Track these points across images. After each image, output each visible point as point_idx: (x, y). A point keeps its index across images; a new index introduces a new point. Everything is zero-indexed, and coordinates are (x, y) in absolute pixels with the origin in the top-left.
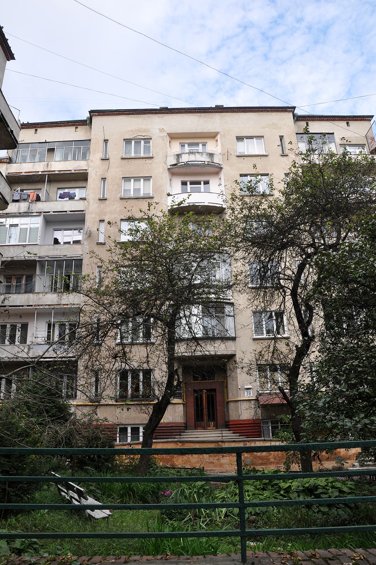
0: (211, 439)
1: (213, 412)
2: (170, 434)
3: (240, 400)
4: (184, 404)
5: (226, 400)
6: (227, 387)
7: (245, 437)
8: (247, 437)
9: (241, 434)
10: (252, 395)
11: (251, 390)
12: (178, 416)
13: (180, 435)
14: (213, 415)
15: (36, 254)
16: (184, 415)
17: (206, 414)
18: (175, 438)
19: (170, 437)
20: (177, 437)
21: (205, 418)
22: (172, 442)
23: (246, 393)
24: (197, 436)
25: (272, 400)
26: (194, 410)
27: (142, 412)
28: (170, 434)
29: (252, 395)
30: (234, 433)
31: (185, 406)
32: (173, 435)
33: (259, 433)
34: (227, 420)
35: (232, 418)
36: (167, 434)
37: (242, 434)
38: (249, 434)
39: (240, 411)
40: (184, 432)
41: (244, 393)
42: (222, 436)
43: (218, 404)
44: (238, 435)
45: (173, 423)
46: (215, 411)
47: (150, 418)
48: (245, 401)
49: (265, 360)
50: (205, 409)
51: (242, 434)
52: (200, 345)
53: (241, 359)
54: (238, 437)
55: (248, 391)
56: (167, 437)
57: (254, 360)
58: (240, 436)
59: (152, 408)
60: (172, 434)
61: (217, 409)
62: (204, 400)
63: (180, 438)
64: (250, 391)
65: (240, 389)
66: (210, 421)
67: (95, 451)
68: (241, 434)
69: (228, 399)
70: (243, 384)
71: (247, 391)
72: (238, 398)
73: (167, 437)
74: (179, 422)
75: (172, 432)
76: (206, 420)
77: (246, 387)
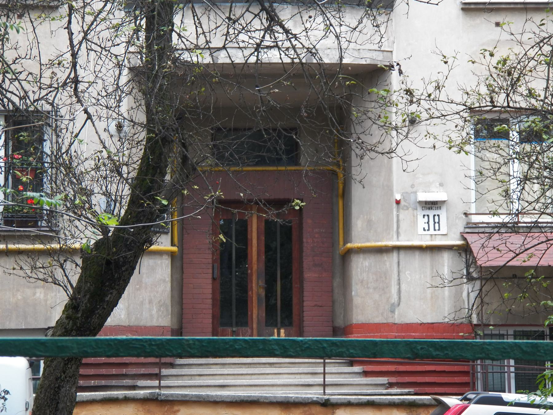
0: (280, 394)
1: (287, 291)
2: (114, 371)
3: (398, 248)
4: (172, 255)
5: (342, 248)
6: (346, 194)
7: (412, 390)
8: (417, 389)
9: (393, 380)
10: (443, 230)
11: (444, 209)
12: (150, 302)
13: (158, 377)
14: (287, 305)
15: (445, 57)
16: (172, 297)
17: (259, 295)
18: (134, 387)
19: (114, 382)
20: (141, 383)
21: (255, 312)
22: (127, 400)
23: (422, 222)
24: (221, 382)
25: (544, 246)
26: (214, 279)
27: (41, 276)
28: (114, 371)
29: (443, 230)
30: (366, 374)
31: (178, 264)
32: (125, 376)
33: (465, 379)
34: (340, 322)
35: (354, 322)
36: (103, 371)
37: (407, 379)
38: (427, 379)
39: (394, 290)
40: (172, 365)
41: (414, 223)
42: (324, 385)
43: (307, 262)
44: (384, 380)
45: (129, 327)
46: (295, 286)
47: (72, 298)
48: (417, 254)
49: (525, 93)
50: (254, 278)
51: (407, 379)
52: (283, 27)
53: (434, 84)
54: (385, 391)
55: (431, 213)
56: (103, 382)
57: (484, 90)
58: (391, 385)
59: (80, 262)
60: (124, 371)
61: (301, 280)
62: (255, 242)
63: (160, 387)
64: (436, 212)
65: (398, 202)
66: (276, 326)
67: (151, 345)
68: (393, 380)
69: (347, 239)
70: (412, 186)
71: (427, 212)
72: (391, 239)
73: (103, 382)
74: (155, 323)
75: (125, 365)
76: (259, 322)
77: (423, 197)
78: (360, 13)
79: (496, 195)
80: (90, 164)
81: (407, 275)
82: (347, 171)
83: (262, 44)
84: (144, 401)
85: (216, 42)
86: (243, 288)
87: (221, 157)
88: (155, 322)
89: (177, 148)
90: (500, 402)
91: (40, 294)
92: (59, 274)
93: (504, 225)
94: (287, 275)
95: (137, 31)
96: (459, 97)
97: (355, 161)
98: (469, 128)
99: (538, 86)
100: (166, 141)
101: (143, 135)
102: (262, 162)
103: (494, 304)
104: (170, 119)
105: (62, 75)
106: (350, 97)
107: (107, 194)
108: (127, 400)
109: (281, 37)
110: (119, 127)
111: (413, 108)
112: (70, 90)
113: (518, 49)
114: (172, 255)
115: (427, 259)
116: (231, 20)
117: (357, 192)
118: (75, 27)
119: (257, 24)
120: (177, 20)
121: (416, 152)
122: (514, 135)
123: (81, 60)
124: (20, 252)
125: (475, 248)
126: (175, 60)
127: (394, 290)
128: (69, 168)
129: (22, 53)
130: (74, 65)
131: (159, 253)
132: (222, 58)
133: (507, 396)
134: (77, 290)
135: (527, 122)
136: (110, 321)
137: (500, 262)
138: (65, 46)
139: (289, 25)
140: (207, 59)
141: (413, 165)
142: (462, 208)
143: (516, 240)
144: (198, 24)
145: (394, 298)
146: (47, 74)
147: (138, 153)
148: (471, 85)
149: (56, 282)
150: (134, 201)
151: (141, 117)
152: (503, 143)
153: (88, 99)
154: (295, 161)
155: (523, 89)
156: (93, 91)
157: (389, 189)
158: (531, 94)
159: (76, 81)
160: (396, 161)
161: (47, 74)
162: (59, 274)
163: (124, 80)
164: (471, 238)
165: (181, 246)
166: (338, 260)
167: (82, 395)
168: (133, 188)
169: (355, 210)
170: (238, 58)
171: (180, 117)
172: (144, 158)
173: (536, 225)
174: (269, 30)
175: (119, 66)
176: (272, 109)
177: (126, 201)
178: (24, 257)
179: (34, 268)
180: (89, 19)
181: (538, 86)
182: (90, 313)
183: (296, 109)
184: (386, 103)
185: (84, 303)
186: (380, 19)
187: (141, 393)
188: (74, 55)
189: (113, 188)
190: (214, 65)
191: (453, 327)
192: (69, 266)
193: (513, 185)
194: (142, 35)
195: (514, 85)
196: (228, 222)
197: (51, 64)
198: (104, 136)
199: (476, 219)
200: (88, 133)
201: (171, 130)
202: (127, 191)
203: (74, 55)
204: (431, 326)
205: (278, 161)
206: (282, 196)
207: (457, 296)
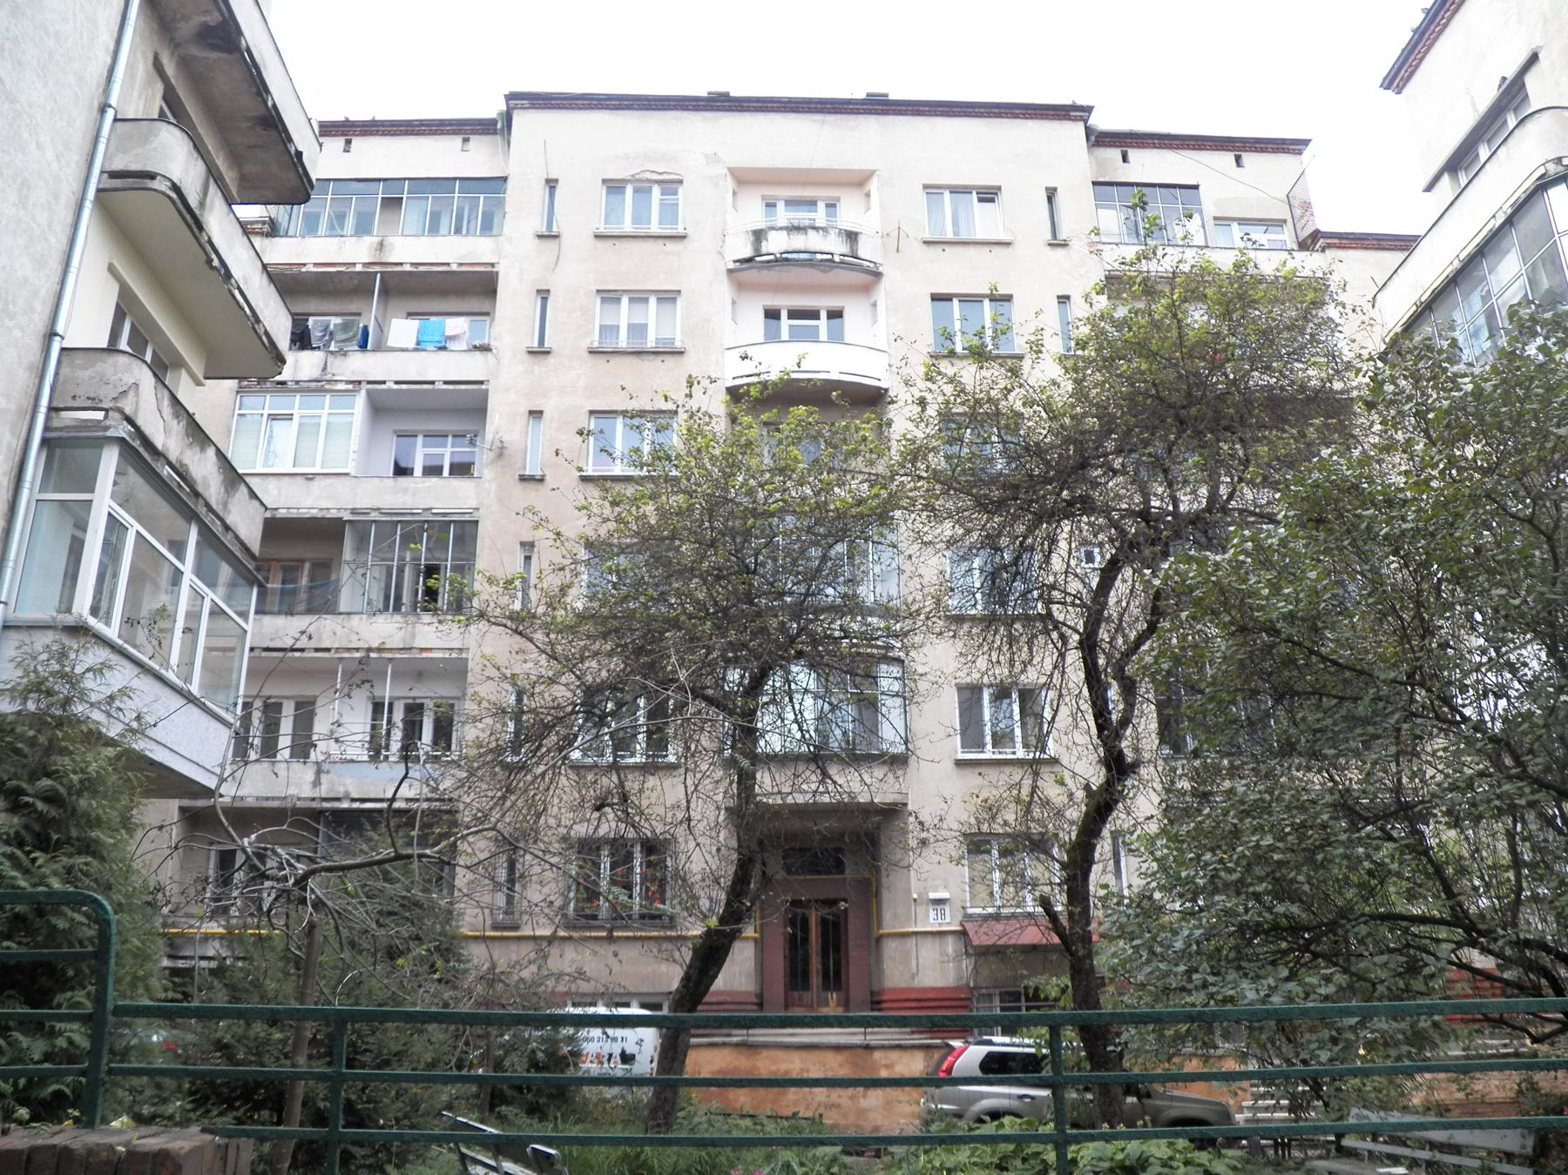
4: (755, 940)
5: (876, 933)
6: (878, 894)
14: (838, 974)
22: (724, 1044)
23: (932, 914)
29: (948, 919)
34: (876, 988)
39: (914, 963)
41: (927, 915)
43: (851, 943)
57: (973, 821)
69: (880, 926)
77: (932, 895)
78: (886, 768)
79: (984, 895)
80: (699, 877)
81: (923, 953)
82: (878, 881)
83: (765, 248)
84: (737, 1045)
85: (786, 789)
86: (806, 961)
87: (789, 871)
88: (744, 989)
89: (758, 866)
90: (990, 1043)
91: (663, 967)
92: (677, 954)
93: (990, 915)
94: (837, 949)
95: (731, 783)
96: (955, 826)
97: (884, 873)
98: (964, 848)
99: (1011, 817)
100: (751, 860)
101: (735, 856)
102: (819, 873)
103: (985, 972)
104: (754, 846)
105: (680, 816)
106: (878, 828)
107: (711, 899)
108: (724, 1044)
109: (831, 788)
110: (718, 850)
111: (924, 835)
112: (685, 826)
113: (995, 792)
114: (755, 940)
115: (937, 940)
116: (796, 776)
117: (885, 894)
118: (689, 782)
119: (813, 778)
120: (758, 776)
121: (926, 867)
122: (995, 853)
123: (692, 805)
124: (641, 938)
125: (971, 934)
126: (757, 804)
127: (914, 963)
128: (684, 880)
129: (653, 800)
130: (688, 808)
131: (747, 939)
132: (790, 800)
133: (995, 1039)
134: (690, 967)
135: (1007, 842)
136: (714, 988)
137: (990, 943)
138: (682, 795)
139: (836, 778)
140: (780, 801)
141: (924, 876)
142: (960, 904)
143: (999, 927)
144: (774, 779)
145: (914, 969)
146: (670, 814)
147: (732, 870)
148: (964, 818)
149: (674, 961)
150: (728, 904)
151: (734, 844)
152: (986, 857)
153: (696, 832)
154: (842, 872)
155: (1000, 820)
156: (701, 826)
157: (909, 892)
158: (1006, 823)
159: (689, 819)
160: (912, 873)
161: (670, 814)
162: (677, 954)
163: (721, 818)
164: (968, 926)
165: (762, 933)
166: (873, 942)
167: (694, 1041)
168: (728, 894)
169: (885, 906)
170: (800, 799)
171: (761, 843)
172: (736, 873)
173: (1014, 916)
174: (822, 782)
175: (718, 808)
176: (824, 837)
177: (723, 904)
178: (652, 943)
179: (660, 951)
180: (699, 776)
181: (1011, 817)
182: (699, 983)
183: (842, 835)
184: (905, 832)
185: (694, 977)
186: (900, 773)
187: (735, 1039)
188: (688, 802)
189: (714, 895)
190: (785, 805)
191: (956, 989)
192: (683, 949)
193: (996, 888)
194: (735, 786)
195: (993, 818)
196: (795, 915)
197: (673, 807)
198: (708, 857)
199: (970, 911)
200: (697, 856)
201: (1106, 942)
202: (723, 896)
203: (688, 802)
204: (942, 989)
205: (830, 873)
206: (832, 896)
207: (959, 968)
